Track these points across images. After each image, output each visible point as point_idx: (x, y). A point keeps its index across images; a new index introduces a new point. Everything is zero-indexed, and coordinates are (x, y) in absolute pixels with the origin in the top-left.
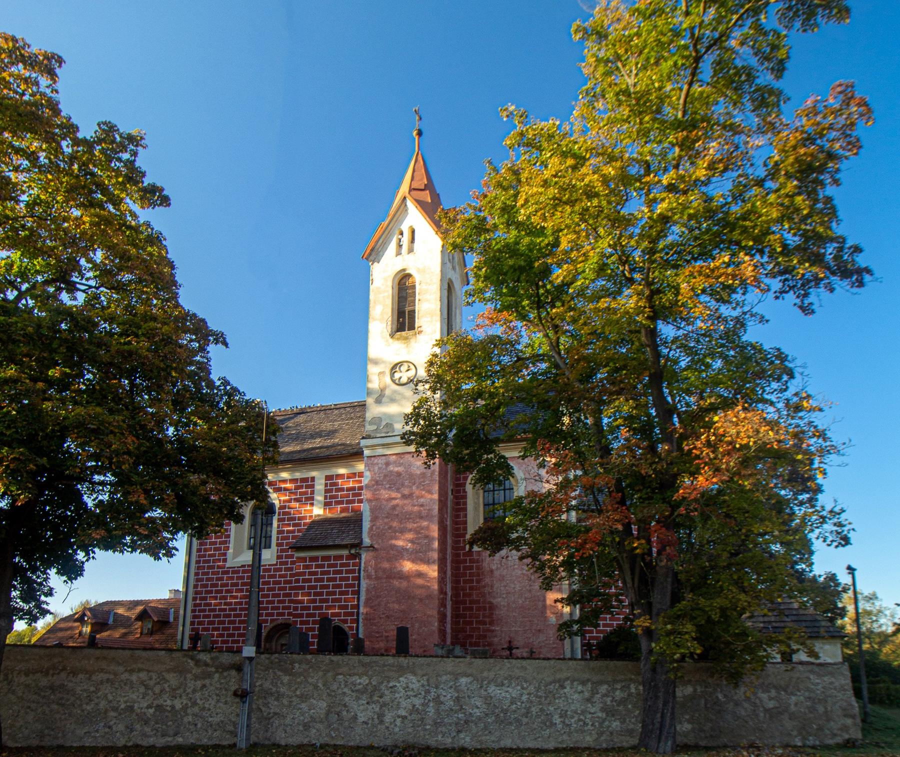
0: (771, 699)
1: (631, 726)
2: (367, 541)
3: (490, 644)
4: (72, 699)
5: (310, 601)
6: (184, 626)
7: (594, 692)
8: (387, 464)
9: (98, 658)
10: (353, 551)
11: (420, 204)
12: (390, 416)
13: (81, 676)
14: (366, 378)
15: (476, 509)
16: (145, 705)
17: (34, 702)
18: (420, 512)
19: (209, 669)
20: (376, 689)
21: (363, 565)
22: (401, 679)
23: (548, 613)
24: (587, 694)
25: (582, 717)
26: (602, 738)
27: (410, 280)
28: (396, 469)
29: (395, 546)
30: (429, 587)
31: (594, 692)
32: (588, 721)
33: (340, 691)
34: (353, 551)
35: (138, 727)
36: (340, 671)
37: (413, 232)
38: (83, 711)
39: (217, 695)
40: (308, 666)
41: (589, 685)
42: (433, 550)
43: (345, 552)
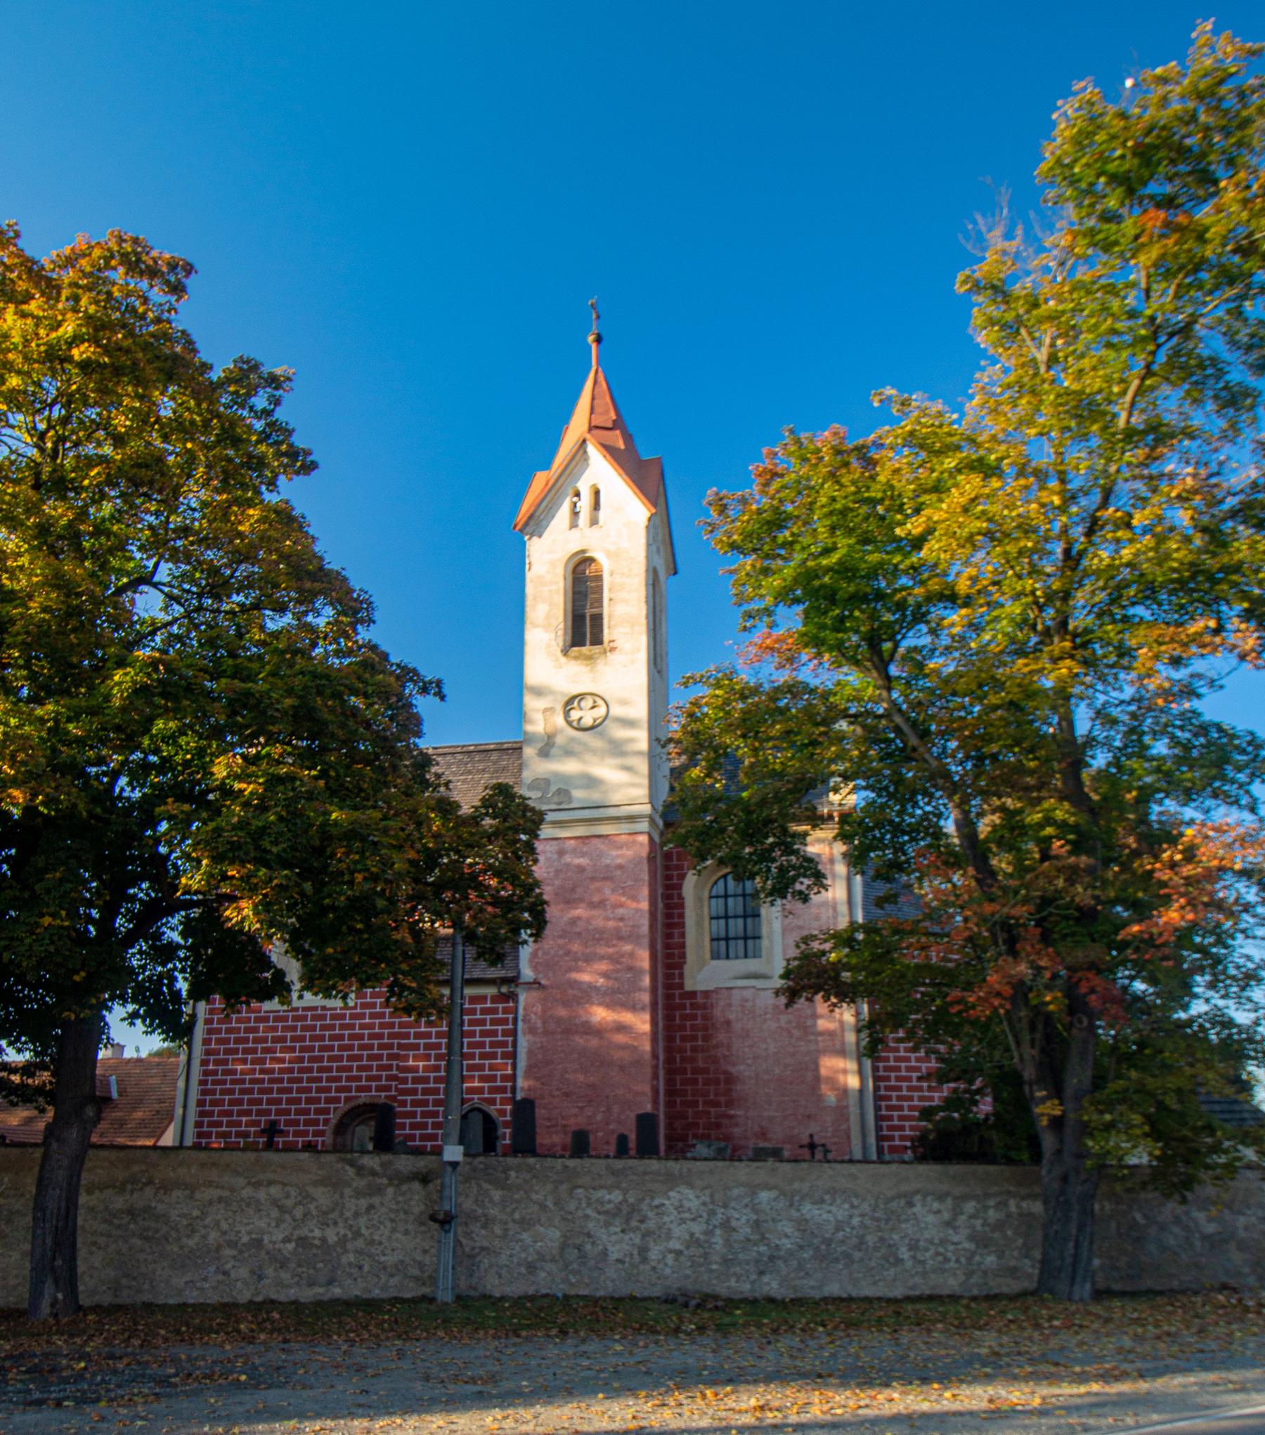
0: (1210, 1220)
1: (1013, 1263)
2: (527, 973)
3: (727, 1138)
4: (165, 1229)
5: (426, 1069)
6: (185, 1107)
7: (956, 1212)
8: (561, 853)
9: (203, 1165)
10: (504, 989)
11: (609, 450)
12: (565, 778)
13: (177, 1193)
14: (520, 715)
15: (699, 924)
16: (281, 1237)
17: (102, 1235)
18: (617, 929)
19: (379, 1181)
20: (634, 1209)
21: (521, 1012)
22: (672, 1194)
23: (824, 1088)
24: (946, 1216)
25: (941, 1250)
26: (973, 1281)
27: (593, 566)
28: (577, 861)
29: (576, 982)
30: (635, 1048)
31: (956, 1212)
32: (949, 1255)
33: (580, 1213)
34: (504, 989)
35: (270, 1272)
36: (580, 1182)
37: (597, 493)
38: (182, 1248)
39: (392, 1221)
40: (528, 1176)
41: (949, 1201)
42: (640, 989)
43: (490, 991)
